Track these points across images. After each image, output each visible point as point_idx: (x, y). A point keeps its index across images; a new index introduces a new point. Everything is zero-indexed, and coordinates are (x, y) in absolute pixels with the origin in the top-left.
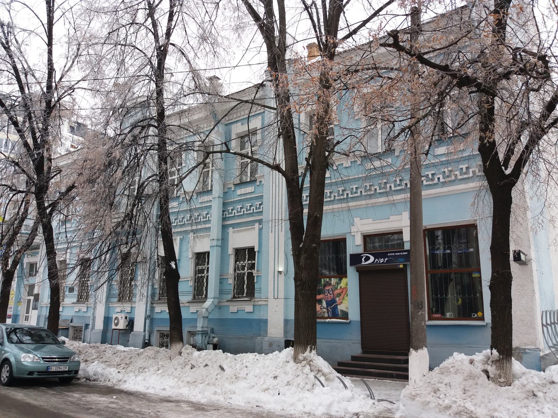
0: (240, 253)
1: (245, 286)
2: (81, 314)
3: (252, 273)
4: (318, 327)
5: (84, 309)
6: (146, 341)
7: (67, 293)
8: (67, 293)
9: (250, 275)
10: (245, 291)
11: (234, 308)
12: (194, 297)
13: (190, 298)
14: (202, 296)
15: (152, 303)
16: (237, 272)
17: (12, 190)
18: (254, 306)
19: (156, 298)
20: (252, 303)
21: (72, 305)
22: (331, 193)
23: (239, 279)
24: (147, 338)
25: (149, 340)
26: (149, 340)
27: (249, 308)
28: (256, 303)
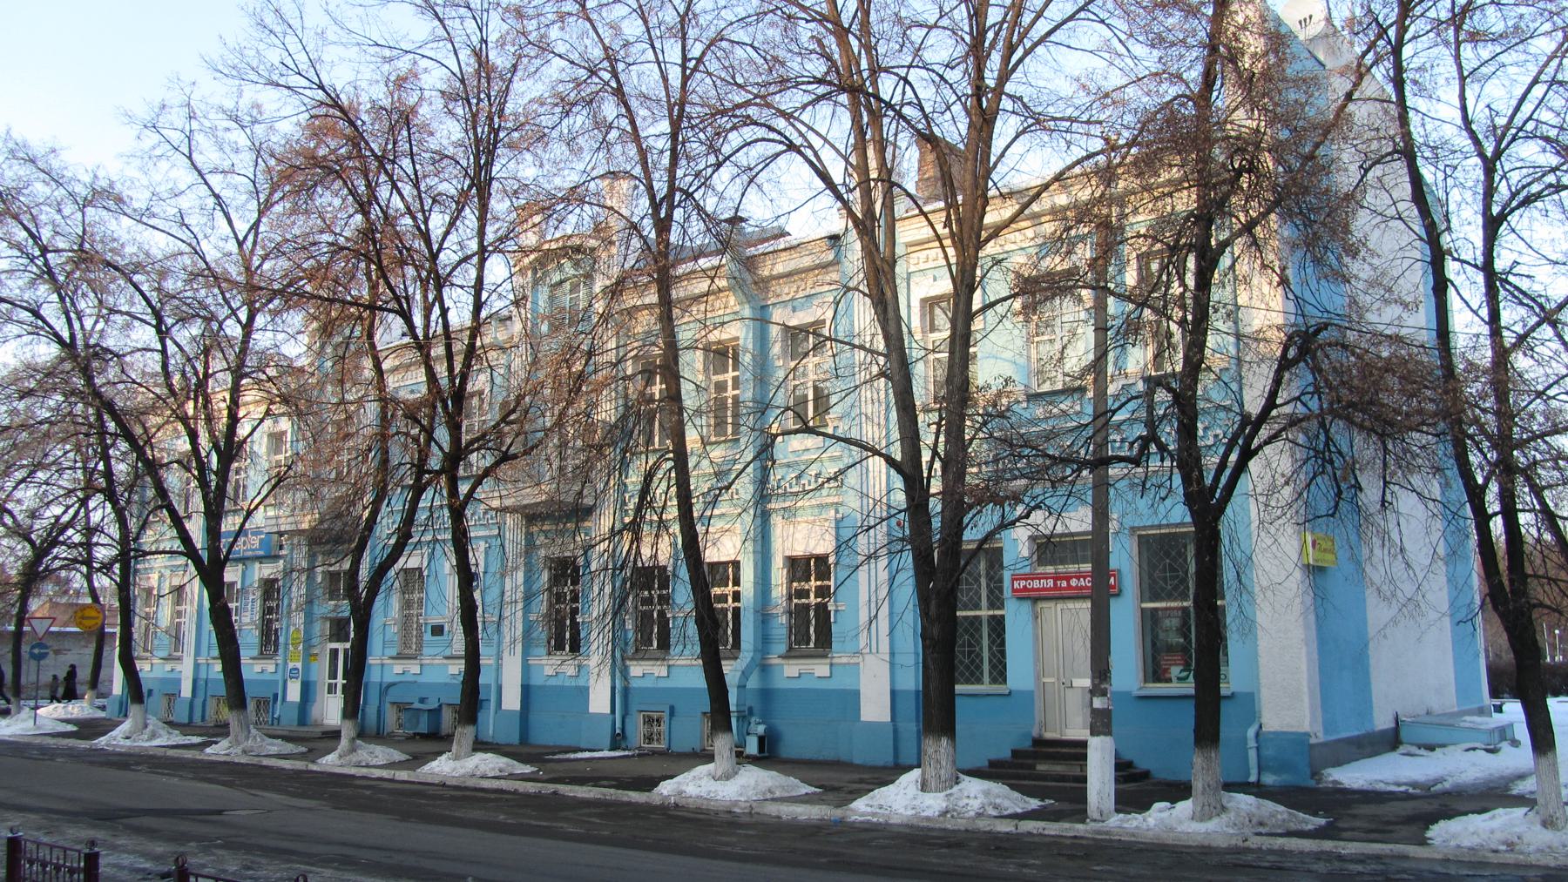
0: (799, 567)
1: (812, 629)
2: (266, 677)
3: (825, 605)
4: (958, 701)
5: (416, 669)
6: (618, 731)
7: (428, 636)
8: (428, 636)
9: (823, 611)
10: (813, 638)
11: (791, 669)
12: (791, 648)
13: (255, 653)
14: (808, 643)
15: (623, 659)
16: (795, 601)
17: (683, 18)
18: (831, 665)
19: (630, 651)
20: (828, 661)
21: (445, 661)
22: (1206, 429)
23: (799, 615)
24: (618, 725)
25: (623, 729)
26: (623, 729)
27: (821, 668)
28: (835, 661)
